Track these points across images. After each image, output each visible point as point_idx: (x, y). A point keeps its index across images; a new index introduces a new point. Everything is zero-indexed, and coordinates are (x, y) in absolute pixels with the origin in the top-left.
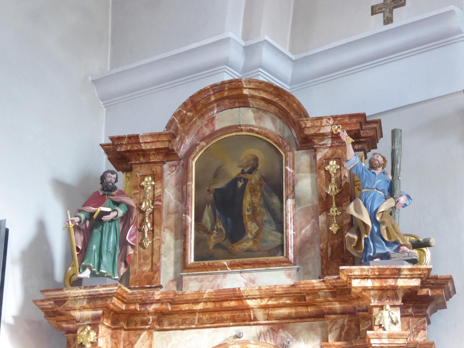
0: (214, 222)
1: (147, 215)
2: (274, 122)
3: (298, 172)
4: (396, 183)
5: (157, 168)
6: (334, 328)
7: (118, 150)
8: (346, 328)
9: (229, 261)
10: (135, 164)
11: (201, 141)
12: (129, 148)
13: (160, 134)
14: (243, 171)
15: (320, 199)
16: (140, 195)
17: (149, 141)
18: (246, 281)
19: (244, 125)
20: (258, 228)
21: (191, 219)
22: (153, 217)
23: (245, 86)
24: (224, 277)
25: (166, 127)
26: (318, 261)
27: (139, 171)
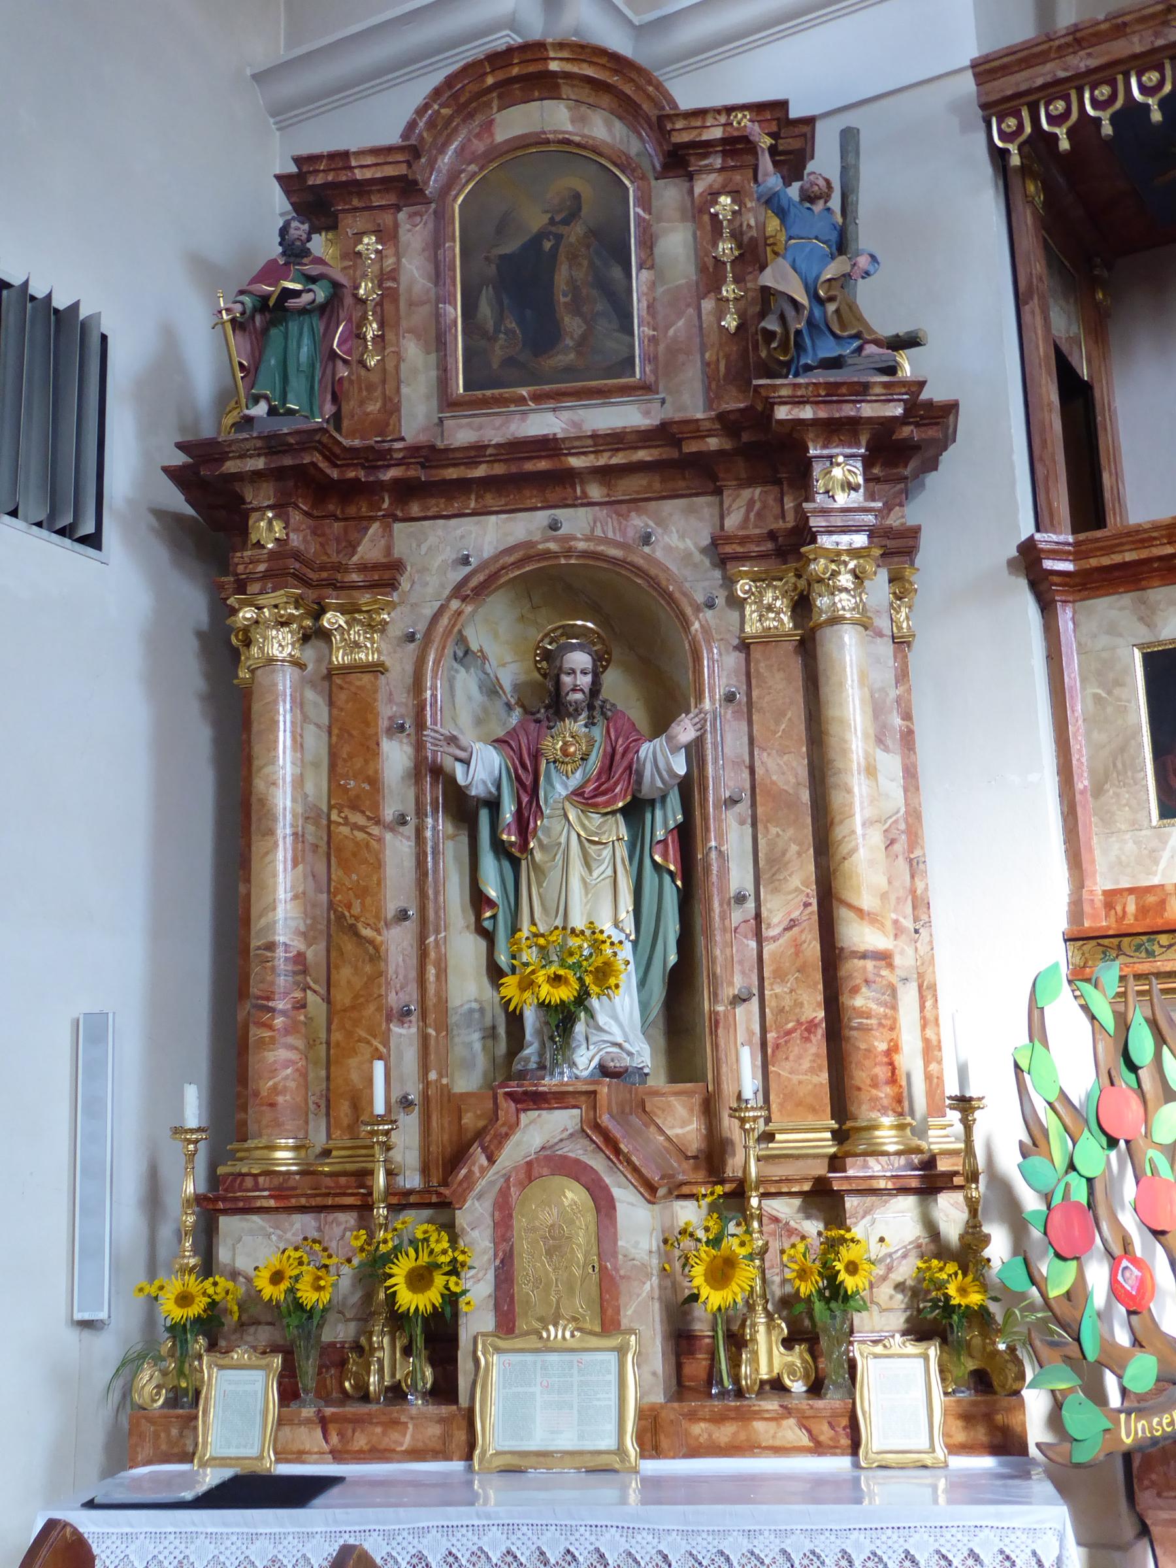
0: (500, 319)
1: (369, 308)
2: (609, 126)
3: (659, 220)
4: (851, 228)
5: (387, 218)
6: (735, 506)
7: (310, 183)
8: (758, 506)
9: (531, 388)
10: (343, 211)
11: (469, 164)
12: (330, 178)
13: (390, 150)
14: (552, 222)
15: (702, 269)
16: (355, 271)
17: (369, 162)
18: (564, 426)
19: (550, 132)
20: (585, 327)
21: (455, 312)
22: (382, 311)
23: (552, 55)
24: (523, 420)
25: (401, 136)
26: (698, 386)
27: (351, 224)
